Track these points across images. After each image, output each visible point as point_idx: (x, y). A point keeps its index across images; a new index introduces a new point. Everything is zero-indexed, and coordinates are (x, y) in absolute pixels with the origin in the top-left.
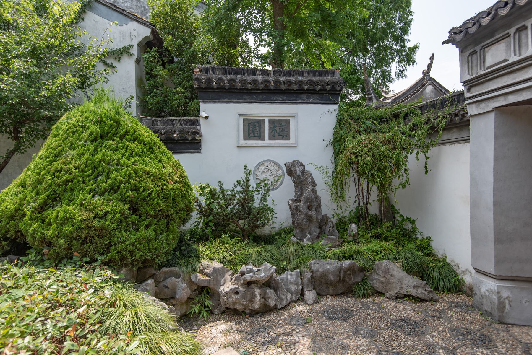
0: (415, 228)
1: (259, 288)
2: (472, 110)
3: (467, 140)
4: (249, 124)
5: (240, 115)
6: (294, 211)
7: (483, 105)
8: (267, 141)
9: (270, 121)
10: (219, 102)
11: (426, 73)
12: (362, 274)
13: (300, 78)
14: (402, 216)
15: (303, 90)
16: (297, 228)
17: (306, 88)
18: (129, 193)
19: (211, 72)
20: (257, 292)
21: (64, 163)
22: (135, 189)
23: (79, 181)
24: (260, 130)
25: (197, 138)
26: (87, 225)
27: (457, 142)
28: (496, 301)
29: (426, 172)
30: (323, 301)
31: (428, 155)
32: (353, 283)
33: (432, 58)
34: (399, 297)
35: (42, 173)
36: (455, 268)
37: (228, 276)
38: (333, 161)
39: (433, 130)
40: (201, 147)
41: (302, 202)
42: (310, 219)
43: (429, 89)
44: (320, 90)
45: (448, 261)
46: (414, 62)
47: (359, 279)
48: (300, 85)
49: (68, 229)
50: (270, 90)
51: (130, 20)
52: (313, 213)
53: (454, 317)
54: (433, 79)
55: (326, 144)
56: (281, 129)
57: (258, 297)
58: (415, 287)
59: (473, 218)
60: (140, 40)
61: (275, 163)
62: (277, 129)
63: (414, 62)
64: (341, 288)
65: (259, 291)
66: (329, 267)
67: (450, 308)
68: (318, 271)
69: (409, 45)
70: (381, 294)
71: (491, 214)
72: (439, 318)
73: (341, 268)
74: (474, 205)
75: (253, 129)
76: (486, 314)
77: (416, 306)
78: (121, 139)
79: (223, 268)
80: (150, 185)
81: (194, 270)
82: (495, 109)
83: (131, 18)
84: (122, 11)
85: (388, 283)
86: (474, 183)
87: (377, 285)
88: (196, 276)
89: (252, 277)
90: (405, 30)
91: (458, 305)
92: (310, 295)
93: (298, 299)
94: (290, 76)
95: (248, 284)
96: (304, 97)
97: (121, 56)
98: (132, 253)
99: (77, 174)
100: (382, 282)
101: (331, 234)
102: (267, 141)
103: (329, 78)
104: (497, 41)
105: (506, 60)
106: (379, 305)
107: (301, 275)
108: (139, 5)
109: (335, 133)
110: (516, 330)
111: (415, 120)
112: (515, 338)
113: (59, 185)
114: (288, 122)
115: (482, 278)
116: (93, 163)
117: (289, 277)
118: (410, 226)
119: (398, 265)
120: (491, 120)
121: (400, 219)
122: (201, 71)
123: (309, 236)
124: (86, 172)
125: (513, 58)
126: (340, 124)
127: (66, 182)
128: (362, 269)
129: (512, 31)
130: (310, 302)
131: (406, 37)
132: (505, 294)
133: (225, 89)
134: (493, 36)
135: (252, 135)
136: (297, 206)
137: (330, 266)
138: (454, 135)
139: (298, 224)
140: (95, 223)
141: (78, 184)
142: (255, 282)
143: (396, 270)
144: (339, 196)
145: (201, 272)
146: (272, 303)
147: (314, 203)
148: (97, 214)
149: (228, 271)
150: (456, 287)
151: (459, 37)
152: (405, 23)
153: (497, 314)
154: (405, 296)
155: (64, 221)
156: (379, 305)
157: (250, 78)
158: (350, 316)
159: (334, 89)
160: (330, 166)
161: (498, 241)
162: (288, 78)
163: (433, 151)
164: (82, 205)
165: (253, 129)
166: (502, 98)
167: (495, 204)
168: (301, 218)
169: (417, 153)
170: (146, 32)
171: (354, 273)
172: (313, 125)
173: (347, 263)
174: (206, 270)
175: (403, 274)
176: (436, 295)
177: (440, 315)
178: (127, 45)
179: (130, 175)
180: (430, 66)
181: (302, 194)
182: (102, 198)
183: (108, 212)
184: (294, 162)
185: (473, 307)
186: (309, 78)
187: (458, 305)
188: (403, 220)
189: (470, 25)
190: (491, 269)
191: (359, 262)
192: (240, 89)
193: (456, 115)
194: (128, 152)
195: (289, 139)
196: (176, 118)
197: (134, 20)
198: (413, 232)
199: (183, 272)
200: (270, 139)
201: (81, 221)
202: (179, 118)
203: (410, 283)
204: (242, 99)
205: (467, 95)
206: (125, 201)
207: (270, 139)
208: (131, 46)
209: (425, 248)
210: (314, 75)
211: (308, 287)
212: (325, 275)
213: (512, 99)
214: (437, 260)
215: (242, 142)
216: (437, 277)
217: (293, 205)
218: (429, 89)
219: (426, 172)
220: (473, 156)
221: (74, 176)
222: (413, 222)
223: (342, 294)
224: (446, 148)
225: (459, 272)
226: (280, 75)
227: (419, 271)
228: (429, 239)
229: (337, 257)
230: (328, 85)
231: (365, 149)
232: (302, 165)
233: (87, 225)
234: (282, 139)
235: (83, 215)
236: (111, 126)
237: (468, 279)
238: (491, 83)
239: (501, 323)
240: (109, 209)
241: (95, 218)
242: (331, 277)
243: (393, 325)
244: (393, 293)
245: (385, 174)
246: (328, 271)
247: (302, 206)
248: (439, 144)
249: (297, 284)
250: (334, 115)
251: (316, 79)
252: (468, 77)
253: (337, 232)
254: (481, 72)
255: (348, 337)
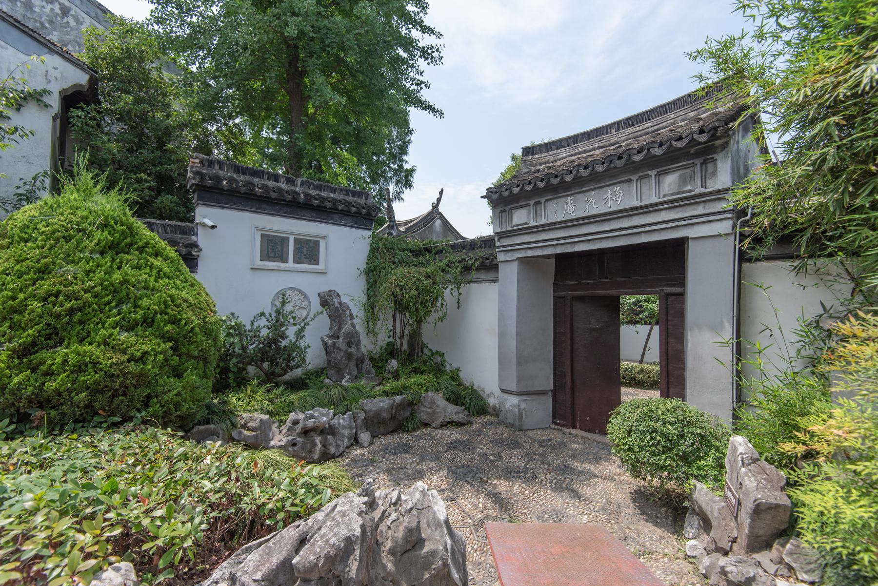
0: (444, 361)
1: (319, 435)
2: (501, 257)
3: (496, 280)
4: (268, 240)
5: (258, 229)
6: (328, 349)
7: (509, 254)
8: (291, 264)
9: (295, 240)
10: (227, 208)
11: (435, 207)
12: (410, 409)
13: (332, 195)
14: (431, 350)
15: (337, 209)
16: (333, 366)
17: (340, 207)
18: (169, 327)
19: (216, 166)
20: (318, 440)
21: (61, 283)
22: (175, 322)
23: (94, 310)
24: (282, 250)
25: (194, 253)
26: (121, 371)
27: (485, 281)
28: (517, 413)
29: (458, 307)
30: (377, 441)
31: (460, 291)
32: (401, 421)
33: (441, 193)
34: (444, 425)
35: (21, 296)
36: (481, 393)
37: (274, 428)
38: (365, 292)
39: (468, 269)
40: (197, 264)
41: (341, 338)
42: (349, 356)
43: (438, 222)
44: (355, 213)
45: (475, 387)
46: (411, 186)
47: (408, 414)
48: (334, 204)
49: (90, 377)
50: (299, 203)
51: (47, 50)
52: (353, 350)
53: (489, 431)
54: (440, 213)
55: (359, 272)
56: (308, 252)
57: (319, 446)
58: (456, 413)
59: (501, 347)
60: (66, 87)
61: (300, 292)
62: (305, 250)
63: (411, 186)
64: (391, 426)
65: (320, 438)
66: (382, 405)
67: (483, 426)
68: (371, 410)
69: (406, 167)
70: (427, 425)
71: (514, 343)
72: (479, 435)
73: (393, 404)
74: (502, 336)
75: (273, 248)
76: (512, 425)
77: (459, 430)
78: (141, 253)
79: (269, 419)
80: (190, 315)
81: (234, 426)
82: (518, 259)
83: (50, 49)
84: (30, 33)
85: (434, 413)
86: (502, 317)
87: (424, 417)
88: (240, 433)
89: (315, 423)
90: (403, 150)
91: (488, 424)
92: (365, 437)
93: (352, 444)
94: (320, 190)
95: (306, 432)
96: (336, 217)
97: (23, 103)
98: (177, 406)
99: (91, 299)
100: (429, 414)
101: (368, 373)
102: (291, 264)
103: (362, 201)
104: (518, 208)
105: (527, 224)
106: (429, 434)
107: (354, 417)
108: (29, 15)
109: (369, 261)
110: (530, 433)
111: (451, 257)
112: (532, 438)
113: (58, 316)
114: (317, 244)
115: (506, 396)
116: (112, 284)
117: (341, 421)
118: (439, 359)
119: (441, 395)
120: (514, 267)
121: (429, 353)
122: (202, 162)
123: (348, 377)
124: (102, 297)
125: (532, 224)
126: (373, 252)
127: (71, 312)
128: (411, 404)
129: (532, 202)
130: (366, 444)
131: (404, 157)
132: (523, 406)
133: (239, 192)
134: (517, 202)
135: (272, 255)
136: (335, 343)
137: (383, 403)
138: (483, 275)
139: (336, 363)
140: (131, 367)
141: (92, 315)
142: (313, 429)
143: (439, 399)
144: (371, 331)
145: (244, 426)
146: (333, 450)
147: (352, 339)
148: (132, 355)
149: (273, 423)
150: (482, 409)
151: (495, 196)
152: (404, 143)
153: (517, 423)
154: (449, 423)
155: (80, 368)
156: (429, 434)
157: (271, 184)
158: (410, 448)
159: (369, 214)
160: (363, 299)
161: (519, 364)
162: (318, 192)
163: (464, 288)
164: (106, 344)
165: (273, 248)
166: (523, 251)
167: (518, 334)
168: (339, 356)
169: (452, 289)
170: (82, 78)
171: (403, 409)
172: (344, 251)
173: (398, 398)
174: (249, 425)
175: (445, 403)
176: (472, 419)
177: (479, 433)
178: (39, 89)
179: (165, 302)
180: (439, 200)
181: (340, 328)
182: (132, 334)
183: (146, 353)
184: (330, 291)
185: (499, 423)
186: (342, 197)
187: (488, 424)
188: (433, 354)
189: (504, 190)
190: (513, 387)
191: (408, 397)
192: (260, 196)
193: (487, 259)
194: (154, 272)
195: (318, 264)
196: (158, 221)
197: (57, 53)
198: (442, 365)
199: (222, 429)
200: (294, 262)
201: (111, 367)
202: (164, 222)
203: (452, 411)
204: (260, 208)
205: (498, 244)
206: (166, 338)
207: (294, 262)
208: (45, 92)
209: (455, 377)
210: (347, 195)
211: (361, 429)
212: (378, 413)
213: (530, 253)
214: (466, 388)
215: (259, 263)
216: (470, 402)
217: (330, 342)
218: (438, 222)
219: (458, 307)
220: (502, 295)
221: (85, 303)
222: (442, 355)
223: (392, 432)
224: (474, 286)
225: (484, 396)
226: (309, 188)
227: (455, 399)
228: (458, 369)
229: (387, 394)
230: (363, 208)
231: (410, 283)
232: (338, 295)
233: (121, 371)
234: (310, 263)
235: (111, 358)
236: (123, 232)
237: (492, 401)
238: (515, 238)
239: (521, 430)
240: (147, 348)
241: (129, 361)
242: (385, 415)
243: (449, 447)
244: (438, 422)
245: (427, 307)
246: (382, 409)
247: (341, 342)
248: (469, 282)
249: (351, 428)
250: (369, 241)
251: (349, 199)
252: (499, 230)
253: (373, 370)
254: (509, 228)
255: (418, 464)
